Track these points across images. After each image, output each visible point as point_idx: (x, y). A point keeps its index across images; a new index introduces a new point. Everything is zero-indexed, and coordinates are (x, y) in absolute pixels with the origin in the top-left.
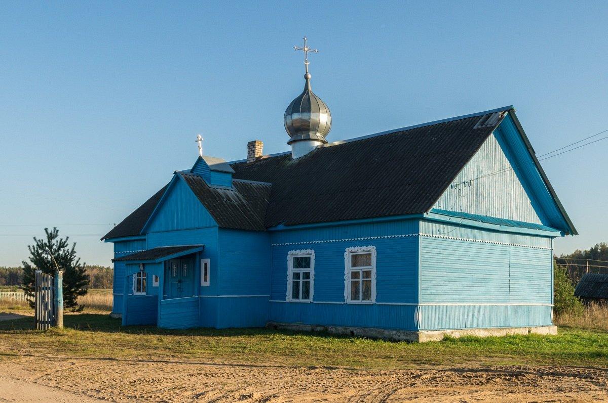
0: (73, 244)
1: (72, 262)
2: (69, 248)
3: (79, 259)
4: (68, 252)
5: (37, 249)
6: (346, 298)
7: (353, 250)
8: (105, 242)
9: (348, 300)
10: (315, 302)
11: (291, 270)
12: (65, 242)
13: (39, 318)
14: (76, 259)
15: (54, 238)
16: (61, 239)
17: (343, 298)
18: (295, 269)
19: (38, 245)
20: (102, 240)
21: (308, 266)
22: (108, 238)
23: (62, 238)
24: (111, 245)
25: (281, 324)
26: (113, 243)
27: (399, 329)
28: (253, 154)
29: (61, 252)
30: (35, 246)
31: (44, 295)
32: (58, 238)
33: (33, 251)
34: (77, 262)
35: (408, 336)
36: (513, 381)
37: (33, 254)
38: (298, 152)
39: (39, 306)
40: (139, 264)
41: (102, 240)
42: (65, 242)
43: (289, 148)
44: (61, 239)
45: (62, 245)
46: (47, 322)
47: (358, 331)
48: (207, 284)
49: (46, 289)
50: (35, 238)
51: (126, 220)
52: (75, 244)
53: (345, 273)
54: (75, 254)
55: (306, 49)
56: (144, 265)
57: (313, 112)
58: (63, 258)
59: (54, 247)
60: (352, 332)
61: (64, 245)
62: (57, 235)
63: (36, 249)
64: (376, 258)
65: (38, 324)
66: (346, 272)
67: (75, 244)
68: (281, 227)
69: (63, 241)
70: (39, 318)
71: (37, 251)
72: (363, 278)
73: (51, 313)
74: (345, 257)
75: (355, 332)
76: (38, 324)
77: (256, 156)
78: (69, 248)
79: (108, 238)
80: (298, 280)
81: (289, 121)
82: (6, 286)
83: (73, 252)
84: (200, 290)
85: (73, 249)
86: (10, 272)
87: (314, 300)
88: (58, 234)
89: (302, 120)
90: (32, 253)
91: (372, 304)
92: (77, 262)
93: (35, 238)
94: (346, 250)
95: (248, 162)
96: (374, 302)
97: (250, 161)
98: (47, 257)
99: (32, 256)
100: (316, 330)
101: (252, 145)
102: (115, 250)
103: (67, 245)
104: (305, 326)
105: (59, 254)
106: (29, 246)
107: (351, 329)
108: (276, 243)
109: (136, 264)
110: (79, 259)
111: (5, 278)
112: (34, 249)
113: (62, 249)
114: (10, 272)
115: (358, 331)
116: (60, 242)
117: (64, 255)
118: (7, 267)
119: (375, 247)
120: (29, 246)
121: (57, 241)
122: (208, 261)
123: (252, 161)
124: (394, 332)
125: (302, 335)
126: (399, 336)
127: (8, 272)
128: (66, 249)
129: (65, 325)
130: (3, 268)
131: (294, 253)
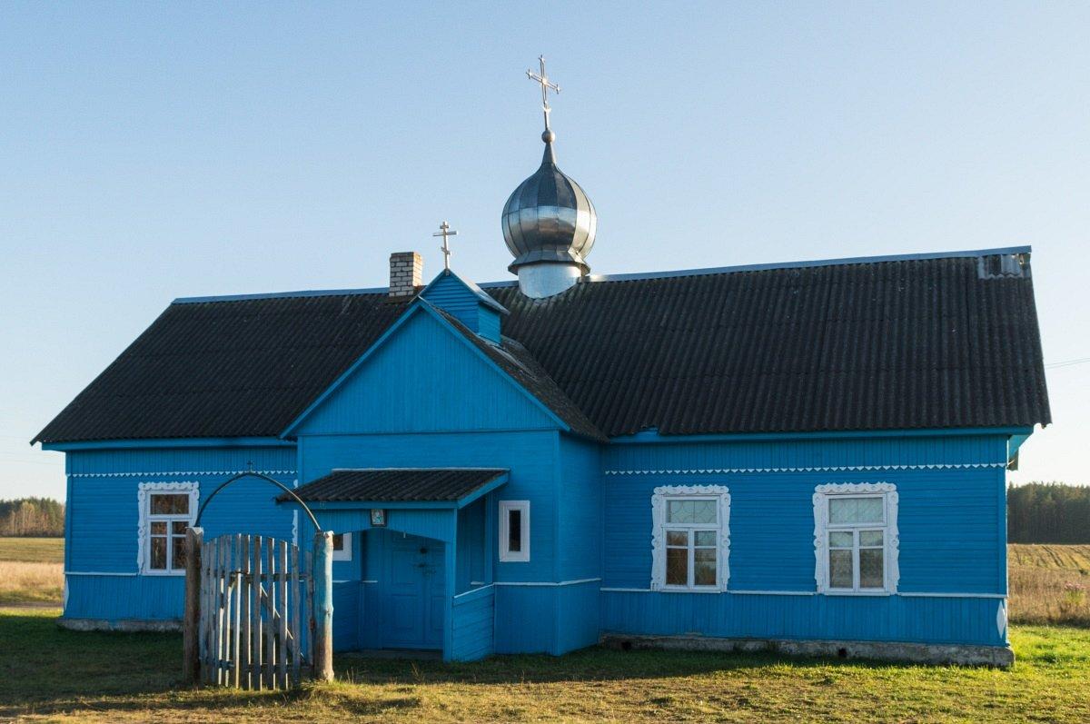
6: (140, 567)
7: (177, 487)
8: (44, 448)
9: (824, 587)
10: (904, 594)
11: (146, 518)
13: (224, 655)
17: (813, 584)
18: (154, 516)
20: (32, 443)
21: (184, 510)
22: (50, 437)
24: (58, 458)
25: (644, 637)
27: (964, 644)
28: (405, 279)
35: (988, 656)
36: (427, 706)
38: (538, 286)
40: (369, 511)
41: (32, 443)
43: (513, 277)
47: (860, 648)
48: (524, 555)
53: (139, 525)
55: (545, 81)
56: (386, 512)
57: (581, 209)
60: (842, 652)
64: (197, 502)
65: (220, 670)
66: (141, 523)
68: (650, 436)
70: (224, 655)
72: (165, 539)
74: (139, 498)
75: (851, 650)
76: (220, 670)
77: (415, 284)
79: (50, 437)
80: (153, 536)
81: (514, 221)
84: (498, 569)
87: (729, 587)
89: (556, 223)
91: (888, 595)
94: (656, 490)
95: (391, 295)
96: (894, 591)
97: (398, 294)
100: (745, 648)
101: (402, 262)
102: (70, 469)
104: (714, 641)
107: (840, 645)
108: (617, 470)
109: (361, 510)
115: (860, 648)
119: (894, 487)
122: (525, 507)
123: (404, 294)
124: (953, 649)
125: (794, 666)
126: (966, 656)
129: (337, 676)
131: (165, 488)
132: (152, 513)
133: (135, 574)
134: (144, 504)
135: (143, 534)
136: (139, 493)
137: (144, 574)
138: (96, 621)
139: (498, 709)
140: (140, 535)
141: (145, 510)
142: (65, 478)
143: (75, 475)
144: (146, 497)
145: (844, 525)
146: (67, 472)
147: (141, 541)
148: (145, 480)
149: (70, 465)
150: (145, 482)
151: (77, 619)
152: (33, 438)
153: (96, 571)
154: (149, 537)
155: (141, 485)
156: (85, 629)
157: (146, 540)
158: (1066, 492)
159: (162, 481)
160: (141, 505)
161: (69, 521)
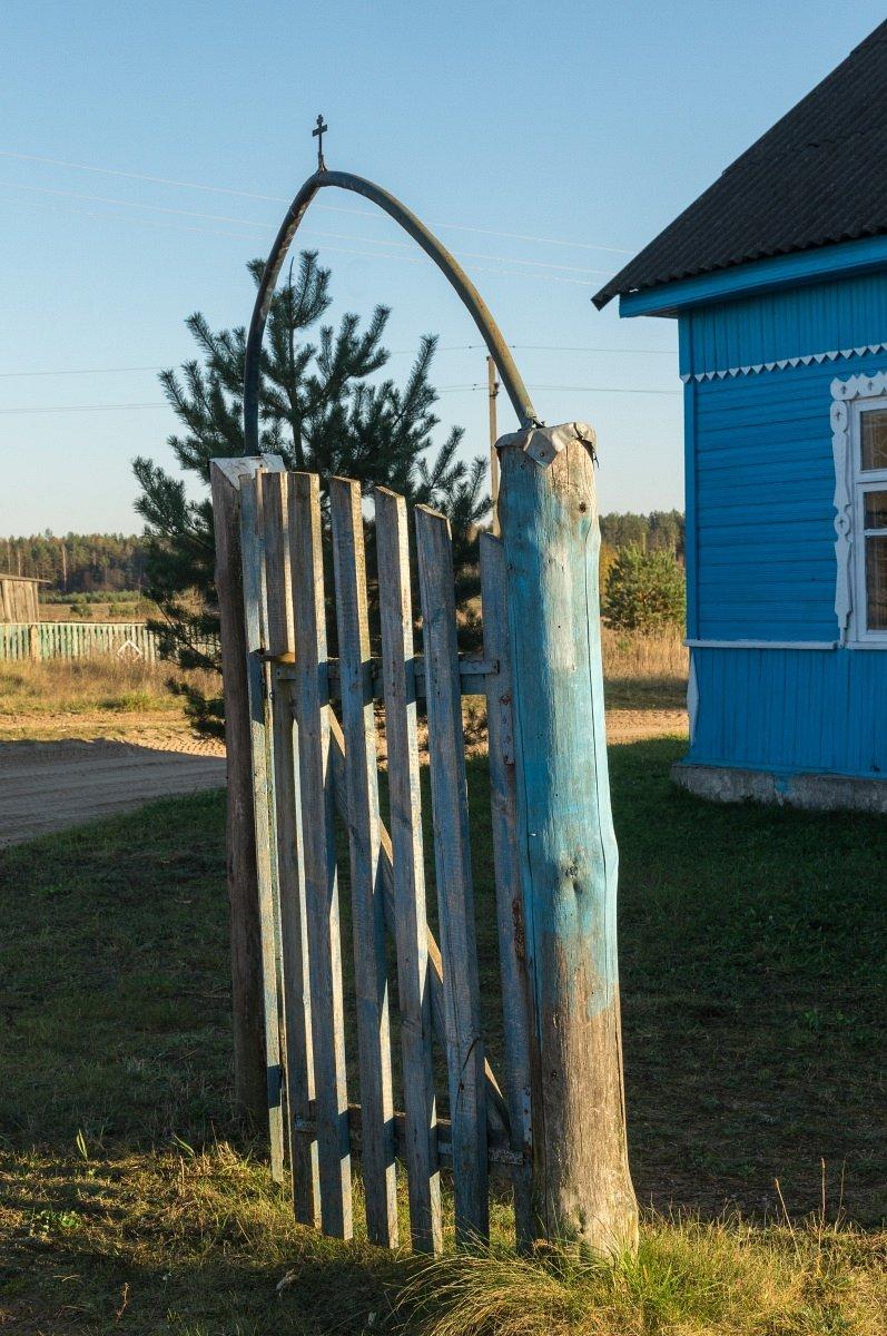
0: (417, 347)
1: (420, 456)
2: (396, 373)
3: (457, 434)
4: (394, 398)
5: (216, 385)
6: (842, 624)
7: (865, 392)
12: (371, 340)
14: (439, 436)
15: (305, 318)
16: (351, 322)
18: (869, 476)
19: (216, 363)
20: (600, 301)
23: (353, 312)
26: (671, 326)
29: (348, 402)
30: (204, 371)
31: (348, 764)
32: (331, 318)
33: (188, 397)
34: (447, 452)
37: (191, 415)
39: (330, 1044)
41: (600, 301)
42: (371, 340)
44: (351, 322)
45: (353, 358)
46: (396, 1140)
49: (372, 687)
50: (196, 323)
51: (729, 172)
52: (430, 344)
54: (431, 409)
58: (366, 434)
59: (312, 370)
61: (365, 354)
62: (321, 302)
63: (207, 387)
67: (430, 344)
69: (360, 333)
71: (216, 397)
73: (457, 1027)
78: (396, 373)
82: (125, 594)
83: (420, 392)
85: (419, 378)
86: (136, 549)
88: (329, 292)
90: (184, 410)
92: (447, 452)
93: (196, 323)
98: (276, 431)
99: (185, 432)
102: (690, 361)
103: (381, 359)
105: (339, 413)
106: (167, 377)
110: (457, 434)
111: (123, 567)
112: (197, 388)
113: (352, 381)
114: (136, 549)
116: (343, 342)
117: (365, 418)
118: (127, 536)
120: (167, 377)
121: (326, 334)
127: (130, 551)
128: (374, 380)
130: (114, 537)
132: (865, 467)
133: (829, 645)
134: (844, 441)
135: (846, 526)
136: (833, 409)
137: (850, 646)
138: (747, 774)
139: (526, 1325)
140: (840, 530)
141: (848, 458)
142: (679, 385)
143: (699, 377)
144: (850, 417)
145: (521, 704)
146: (682, 373)
147: (841, 549)
148: (845, 369)
149: (687, 341)
150: (844, 376)
151: (709, 768)
152: (602, 285)
153: (751, 638)
154: (861, 535)
155: (836, 386)
156: (727, 797)
157: (853, 547)
158: (101, 542)
159: (857, 372)
160: (838, 444)
161: (693, 508)
